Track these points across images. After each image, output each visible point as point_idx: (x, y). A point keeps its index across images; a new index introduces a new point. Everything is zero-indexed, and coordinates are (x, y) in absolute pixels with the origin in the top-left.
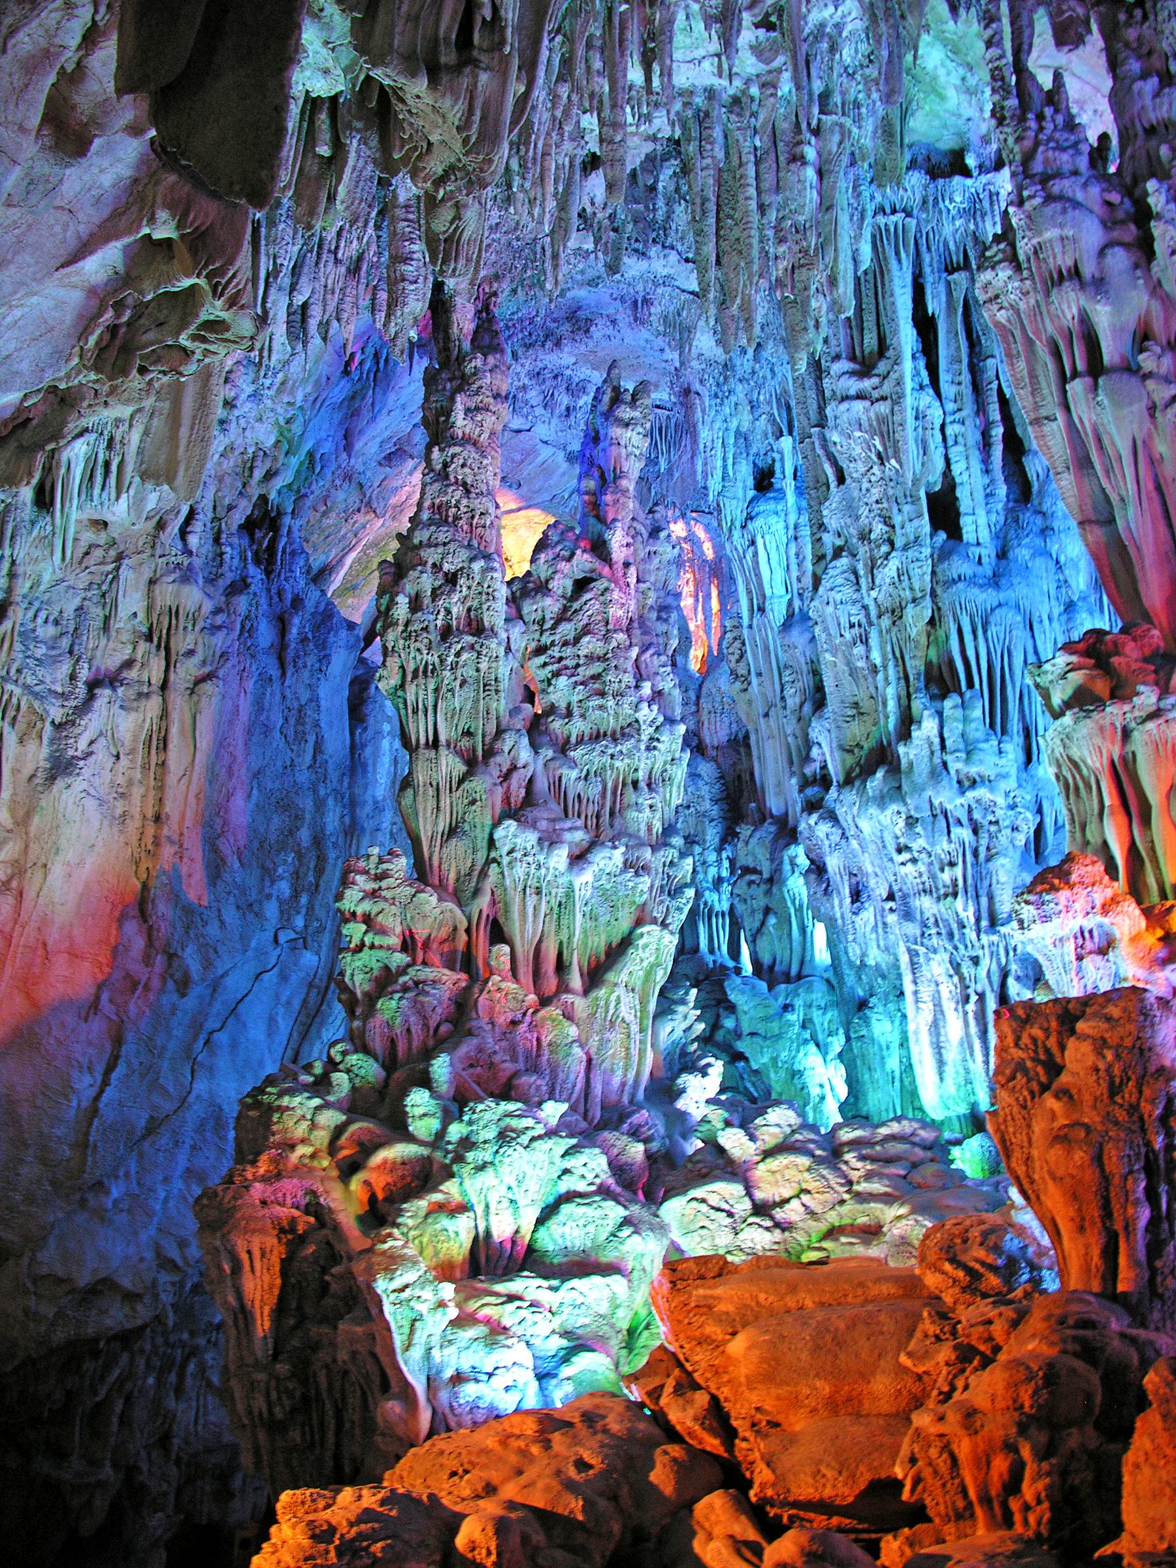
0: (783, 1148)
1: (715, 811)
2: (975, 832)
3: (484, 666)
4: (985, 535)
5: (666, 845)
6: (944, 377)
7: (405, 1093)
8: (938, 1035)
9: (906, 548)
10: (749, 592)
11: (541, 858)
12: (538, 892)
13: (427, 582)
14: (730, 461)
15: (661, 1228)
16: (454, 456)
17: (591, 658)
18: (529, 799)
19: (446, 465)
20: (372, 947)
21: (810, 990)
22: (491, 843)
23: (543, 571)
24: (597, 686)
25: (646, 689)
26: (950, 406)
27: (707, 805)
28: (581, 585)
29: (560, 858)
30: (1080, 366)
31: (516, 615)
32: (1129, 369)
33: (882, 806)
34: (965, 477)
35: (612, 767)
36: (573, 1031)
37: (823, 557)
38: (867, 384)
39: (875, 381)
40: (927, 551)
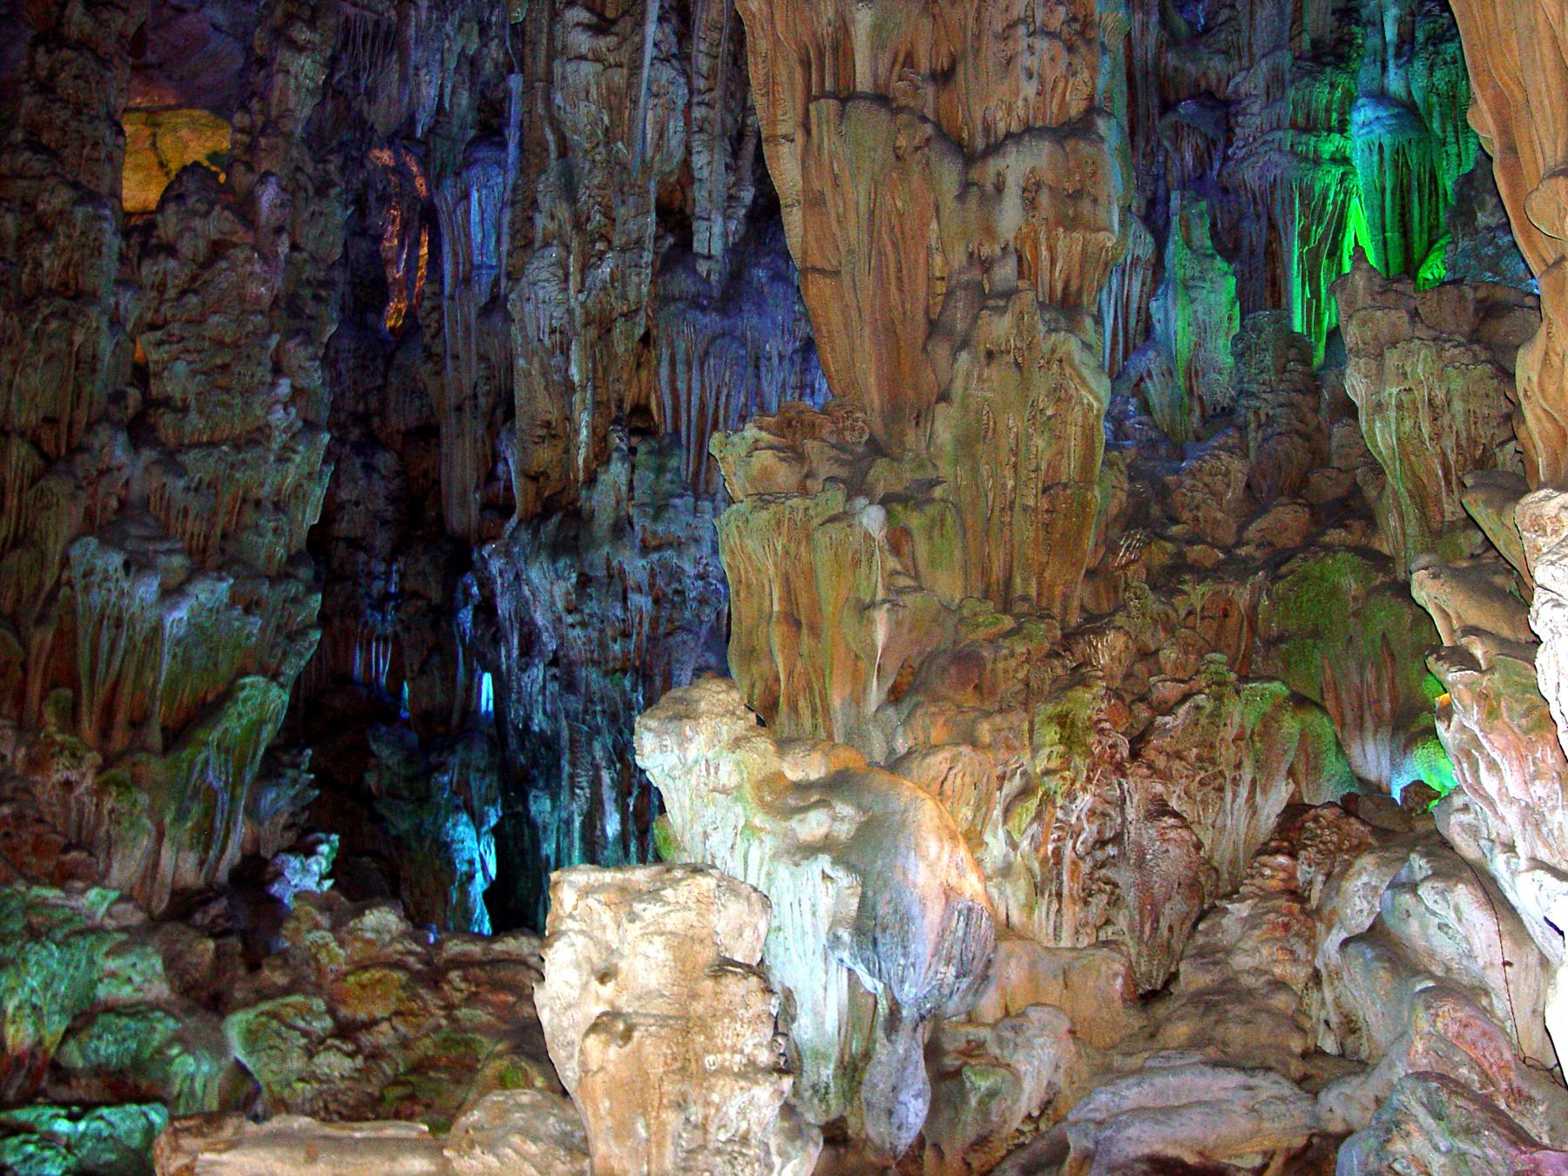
1: (390, 512)
3: (79, 338)
4: (717, 248)
9: (623, 250)
10: (456, 254)
11: (126, 585)
12: (119, 624)
14: (448, 91)
15: (219, 1048)
16: (65, 63)
19: (53, 75)
21: (469, 748)
22: (65, 562)
25: (284, 387)
26: (701, 84)
27: (380, 504)
28: (218, 249)
29: (147, 589)
32: (881, 98)
34: (705, 173)
35: (230, 478)
36: (144, 799)
38: (603, 43)
40: (648, 257)
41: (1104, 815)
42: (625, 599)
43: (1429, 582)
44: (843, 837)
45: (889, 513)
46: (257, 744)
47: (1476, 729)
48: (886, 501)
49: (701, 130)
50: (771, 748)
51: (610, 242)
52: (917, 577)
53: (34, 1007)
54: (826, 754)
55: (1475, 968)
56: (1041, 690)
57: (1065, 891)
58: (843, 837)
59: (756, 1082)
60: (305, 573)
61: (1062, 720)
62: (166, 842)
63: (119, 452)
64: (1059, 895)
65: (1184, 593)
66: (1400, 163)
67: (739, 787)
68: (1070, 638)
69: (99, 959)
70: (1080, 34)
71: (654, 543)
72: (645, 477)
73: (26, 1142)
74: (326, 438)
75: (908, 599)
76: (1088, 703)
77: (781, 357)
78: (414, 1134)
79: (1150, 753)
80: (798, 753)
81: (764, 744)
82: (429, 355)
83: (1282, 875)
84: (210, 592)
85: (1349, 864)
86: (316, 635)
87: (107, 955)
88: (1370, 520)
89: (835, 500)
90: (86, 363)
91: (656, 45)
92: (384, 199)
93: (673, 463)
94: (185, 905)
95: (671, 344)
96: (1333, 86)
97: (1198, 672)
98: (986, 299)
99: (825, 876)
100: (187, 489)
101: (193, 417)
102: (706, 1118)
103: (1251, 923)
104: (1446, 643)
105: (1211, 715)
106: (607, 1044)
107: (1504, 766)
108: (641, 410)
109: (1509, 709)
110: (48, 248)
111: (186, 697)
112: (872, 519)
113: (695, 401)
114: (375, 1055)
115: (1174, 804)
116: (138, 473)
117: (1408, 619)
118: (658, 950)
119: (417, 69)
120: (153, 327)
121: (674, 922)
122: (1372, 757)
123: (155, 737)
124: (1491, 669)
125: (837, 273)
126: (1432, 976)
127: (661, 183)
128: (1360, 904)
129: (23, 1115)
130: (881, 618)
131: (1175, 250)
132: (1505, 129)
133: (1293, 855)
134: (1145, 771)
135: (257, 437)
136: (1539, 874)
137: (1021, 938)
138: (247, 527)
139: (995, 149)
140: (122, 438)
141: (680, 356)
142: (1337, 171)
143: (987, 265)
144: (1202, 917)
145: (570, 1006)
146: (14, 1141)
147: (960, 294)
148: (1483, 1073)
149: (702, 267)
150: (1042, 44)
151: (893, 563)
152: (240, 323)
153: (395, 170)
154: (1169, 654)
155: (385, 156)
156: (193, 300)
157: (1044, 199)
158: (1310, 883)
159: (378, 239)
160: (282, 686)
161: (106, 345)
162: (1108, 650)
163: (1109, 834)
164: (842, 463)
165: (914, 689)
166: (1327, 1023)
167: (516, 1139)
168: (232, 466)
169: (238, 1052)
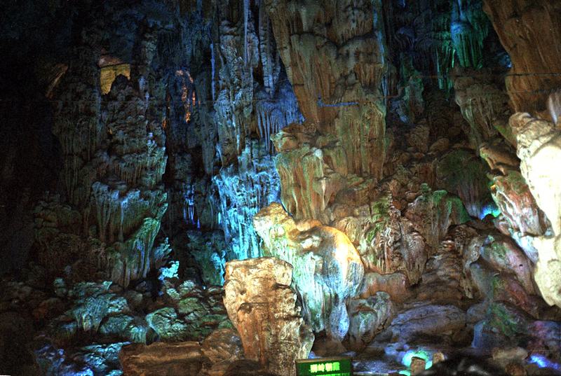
0: (189, 295)
1: (190, 171)
2: (262, 186)
3: (91, 126)
4: (271, 84)
5: (157, 189)
6: (261, 28)
7: (54, 279)
8: (250, 252)
9: (245, 88)
12: (108, 206)
13: (69, 96)
15: (145, 324)
17: (131, 124)
18: (107, 175)
20: (46, 227)
22: (92, 190)
23: (115, 93)
24: (132, 134)
27: (187, 169)
28: (129, 98)
29: (116, 195)
30: (296, 31)
31: (104, 108)
32: (311, 32)
33: (232, 176)
36: (119, 255)
37: (219, 89)
38: (233, 29)
39: (235, 28)
41: (395, 234)
42: (253, 186)
43: (485, 151)
44: (316, 246)
45: (323, 152)
46: (152, 238)
47: (504, 195)
48: (322, 148)
49: (263, 52)
50: (293, 222)
51: (240, 86)
52: (333, 169)
53: (91, 317)
54: (309, 222)
55: (512, 267)
56: (373, 198)
57: (386, 257)
58: (316, 246)
59: (291, 320)
60: (162, 187)
61: (380, 206)
62: (127, 268)
63: (105, 157)
64: (384, 259)
65: (413, 167)
66: (467, 39)
67: (284, 235)
68: (380, 182)
69: (108, 302)
70: (368, 7)
71: (260, 170)
72: (255, 151)
73: (91, 355)
74: (164, 149)
75: (331, 176)
76: (388, 201)
77: (292, 113)
78: (194, 345)
79: (407, 214)
80: (301, 223)
81: (291, 221)
82: (196, 126)
83: (450, 246)
84: (134, 195)
85: (470, 241)
86: (167, 205)
87: (110, 300)
88: (468, 142)
89: (306, 149)
90: (93, 133)
91: (248, 28)
92: (182, 84)
93: (263, 146)
94: (134, 284)
95: (260, 113)
96: (444, 18)
97: (419, 189)
98: (347, 86)
99: (312, 258)
100: (125, 166)
101: (125, 145)
102: (277, 333)
103: (441, 261)
104: (492, 168)
105: (425, 201)
106: (244, 313)
107: (514, 204)
108: (254, 133)
109: (514, 186)
110: (80, 101)
111: (130, 223)
112: (318, 154)
113: (268, 128)
114: (190, 323)
115: (416, 229)
116: (111, 163)
117: (481, 167)
118: (257, 283)
119: (185, 45)
120: (112, 122)
121: (261, 274)
122: (473, 209)
123: (121, 237)
124: (507, 175)
125: (303, 85)
126: (498, 271)
127: (253, 68)
128: (474, 252)
129: (90, 348)
130: (323, 182)
131: (404, 70)
132: (494, 10)
133: (453, 240)
134: (406, 220)
135: (145, 149)
136: (528, 237)
137: (374, 272)
138: (143, 176)
139: (346, 44)
140: (105, 153)
141: (263, 115)
142: (448, 42)
143: (346, 77)
144: (428, 261)
145: (234, 302)
146: (87, 355)
147: (340, 86)
148: (517, 299)
149: (267, 90)
150: (356, 12)
151: (326, 166)
152: (136, 118)
153: (183, 76)
154: (411, 185)
155: (180, 72)
156: (122, 113)
157: (361, 56)
158: (459, 248)
159: (181, 95)
160: (157, 220)
161: (99, 128)
162: (392, 186)
163: (397, 239)
164: (309, 138)
165: (335, 202)
166: (469, 289)
167: (222, 344)
168: (138, 159)
169: (151, 325)
